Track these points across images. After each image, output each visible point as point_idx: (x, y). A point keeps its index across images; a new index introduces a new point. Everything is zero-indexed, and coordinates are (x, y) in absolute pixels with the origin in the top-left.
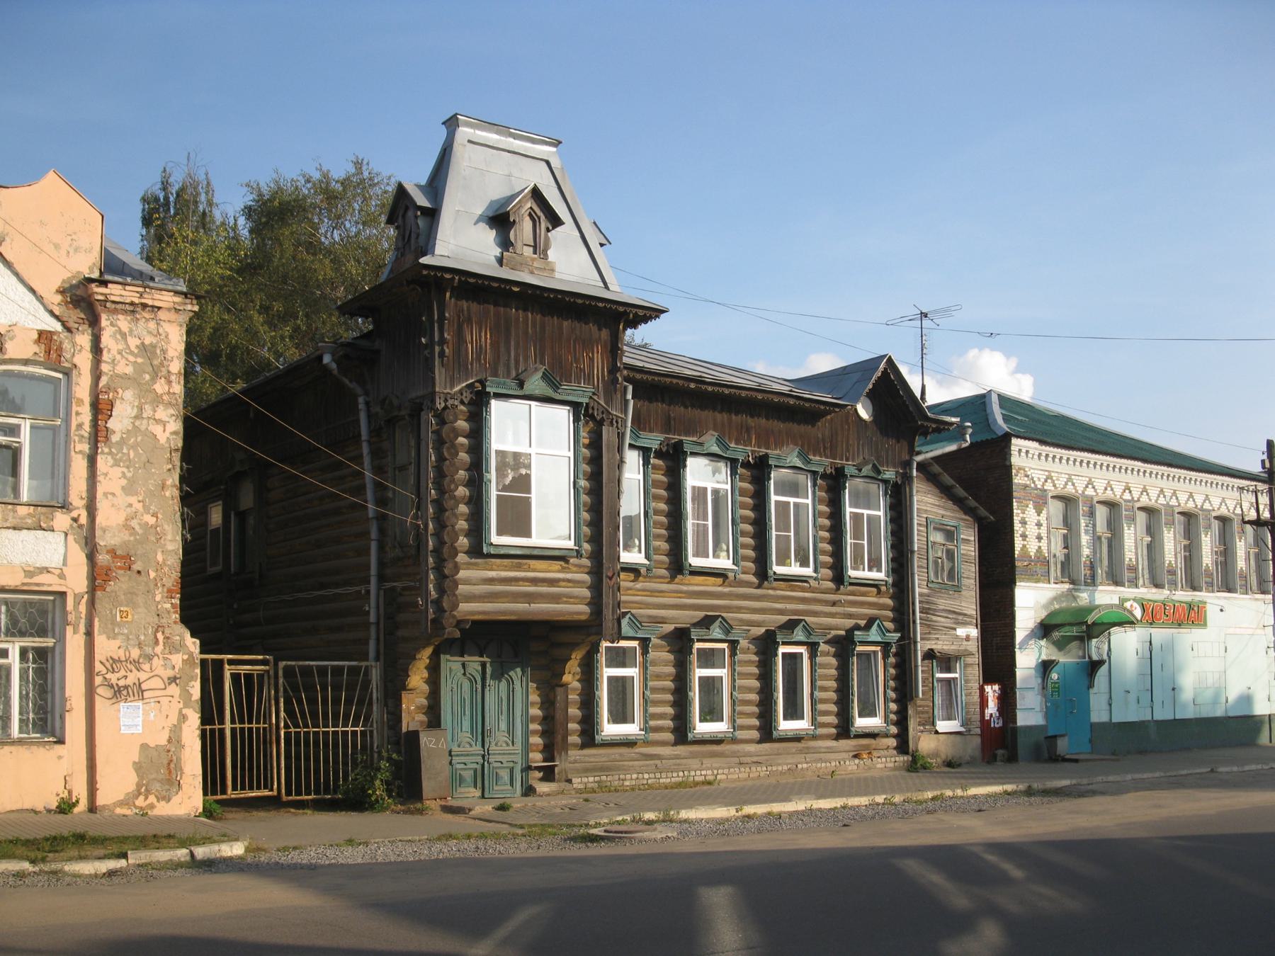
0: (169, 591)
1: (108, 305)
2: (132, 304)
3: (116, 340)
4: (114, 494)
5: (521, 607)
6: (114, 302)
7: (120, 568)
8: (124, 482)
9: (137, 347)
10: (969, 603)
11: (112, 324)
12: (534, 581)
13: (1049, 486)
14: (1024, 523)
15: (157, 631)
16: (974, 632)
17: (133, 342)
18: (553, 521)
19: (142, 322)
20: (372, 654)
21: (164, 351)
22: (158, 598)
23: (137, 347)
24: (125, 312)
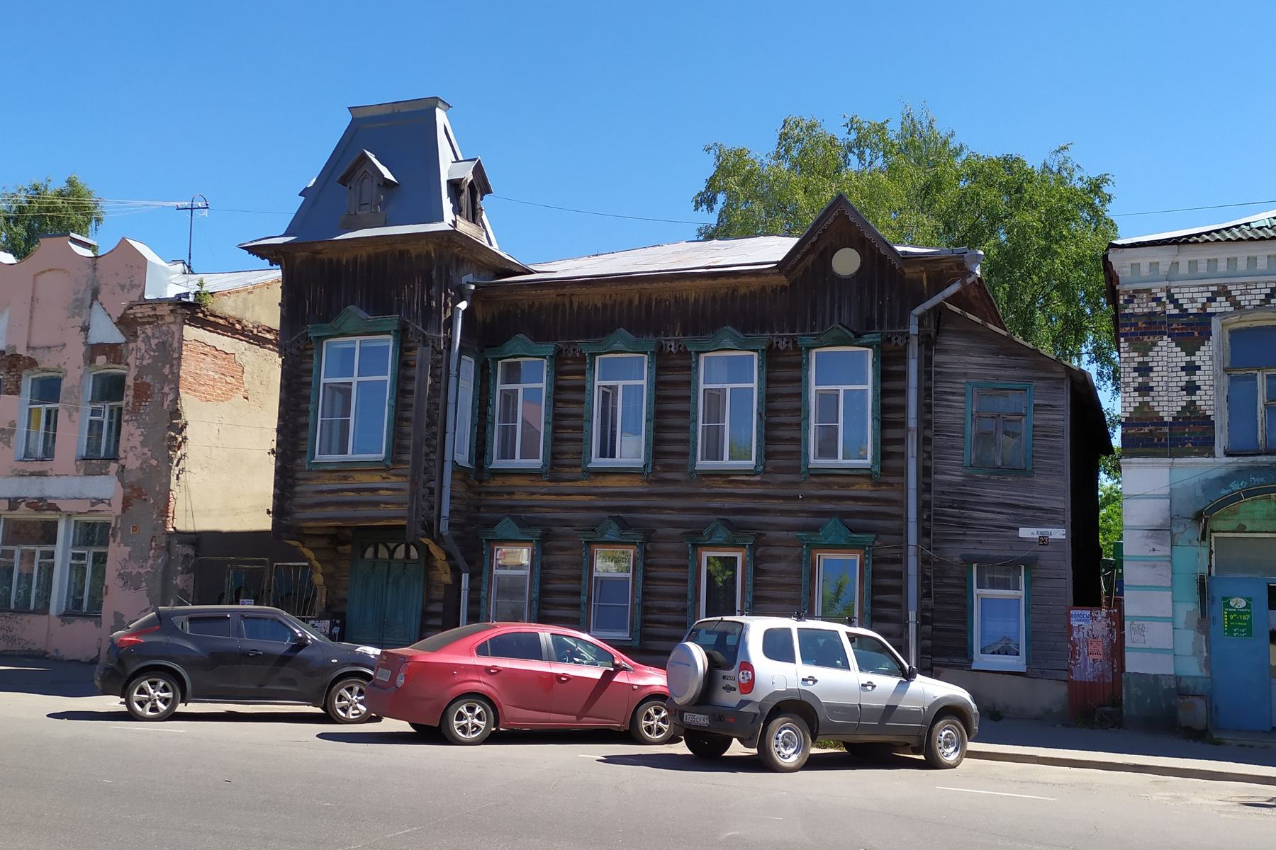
5: (347, 512)
16: (1058, 534)
17: (154, 342)
24: (149, 323)
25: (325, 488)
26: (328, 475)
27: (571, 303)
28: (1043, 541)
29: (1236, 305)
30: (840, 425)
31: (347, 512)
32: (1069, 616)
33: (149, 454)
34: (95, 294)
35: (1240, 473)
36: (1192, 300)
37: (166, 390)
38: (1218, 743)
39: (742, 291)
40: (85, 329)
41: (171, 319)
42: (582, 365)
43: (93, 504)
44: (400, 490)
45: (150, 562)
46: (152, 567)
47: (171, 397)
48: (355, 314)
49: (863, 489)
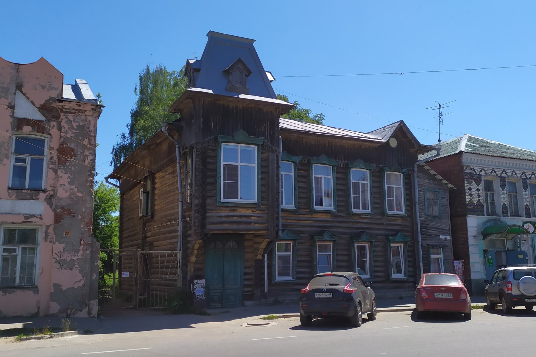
0: (87, 223)
1: (64, 110)
2: (74, 109)
3: (67, 123)
4: (64, 185)
5: (234, 227)
6: (66, 109)
7: (66, 214)
8: (69, 180)
9: (76, 126)
10: (446, 224)
11: (66, 118)
12: (240, 217)
13: (483, 173)
14: (470, 189)
15: (81, 240)
16: (449, 237)
17: (75, 125)
18: (248, 192)
19: (79, 117)
20: (178, 248)
21: (88, 128)
22: (82, 226)
23: (76, 126)
24: (71, 113)
25: (223, 214)
26: (224, 209)
27: (302, 141)
28: (445, 239)
29: (486, 173)
30: (360, 196)
31: (234, 227)
32: (453, 263)
33: (76, 190)
34: (19, 87)
35: (489, 220)
36: (478, 170)
37: (87, 153)
38: (210, 315)
39: (363, 147)
40: (12, 107)
41: (91, 113)
42: (381, 172)
43: (26, 218)
44: (261, 217)
45: (81, 253)
46: (82, 255)
47: (91, 158)
48: (241, 134)
49: (399, 222)
